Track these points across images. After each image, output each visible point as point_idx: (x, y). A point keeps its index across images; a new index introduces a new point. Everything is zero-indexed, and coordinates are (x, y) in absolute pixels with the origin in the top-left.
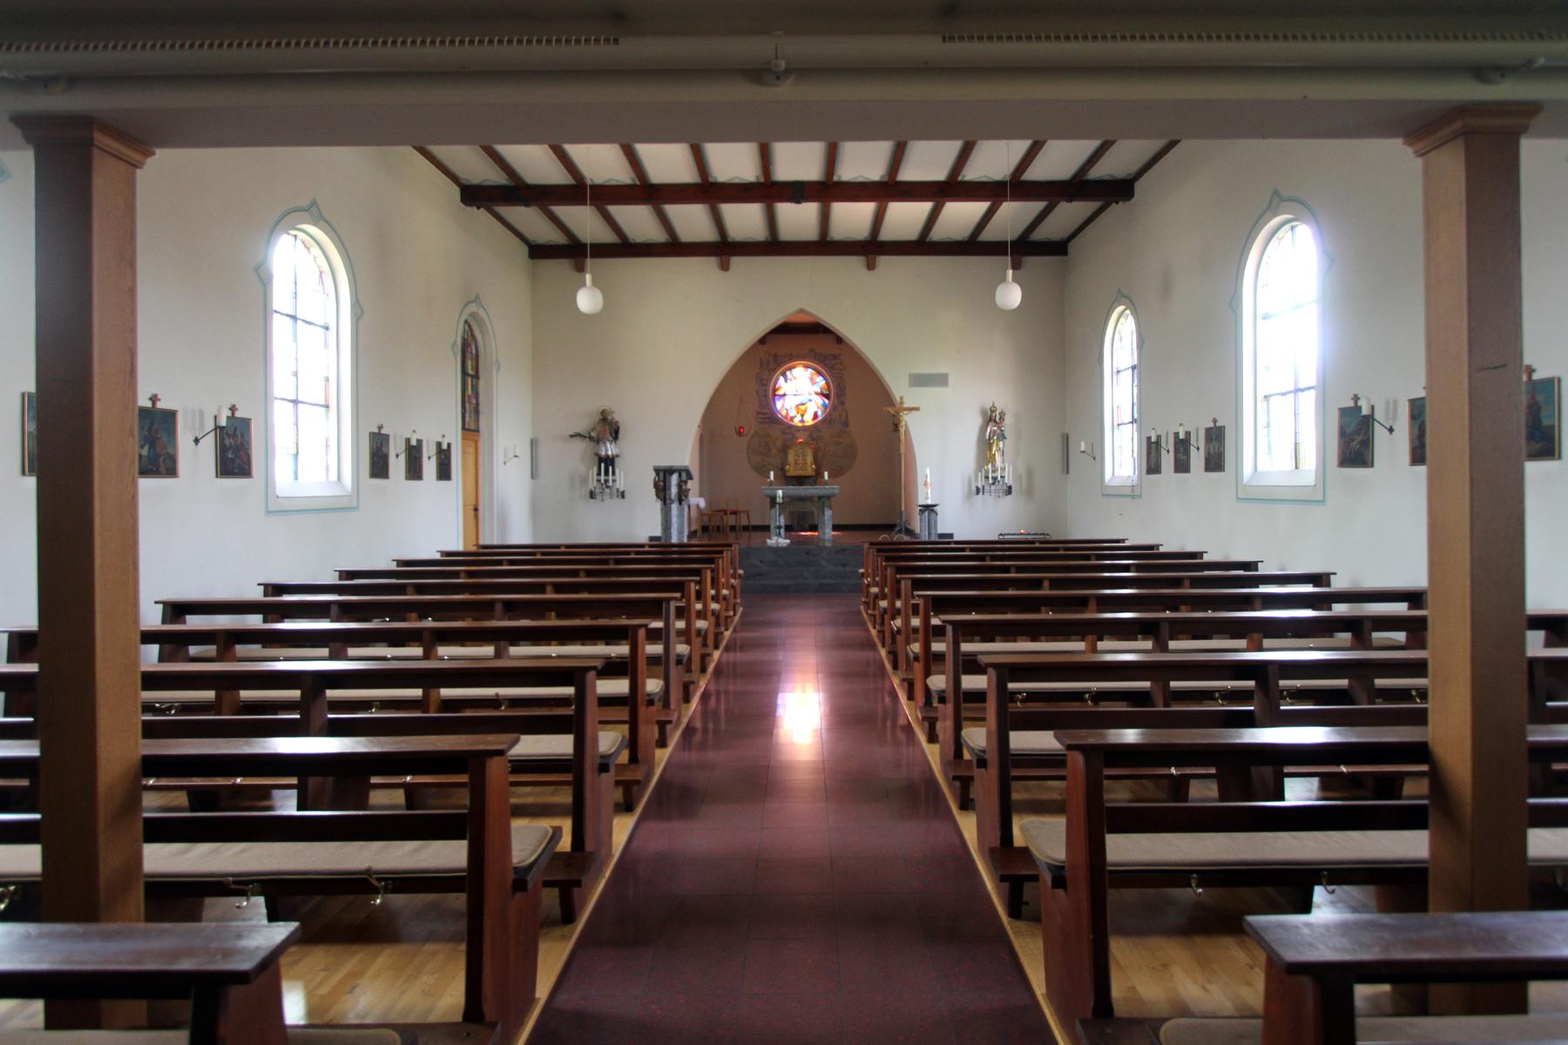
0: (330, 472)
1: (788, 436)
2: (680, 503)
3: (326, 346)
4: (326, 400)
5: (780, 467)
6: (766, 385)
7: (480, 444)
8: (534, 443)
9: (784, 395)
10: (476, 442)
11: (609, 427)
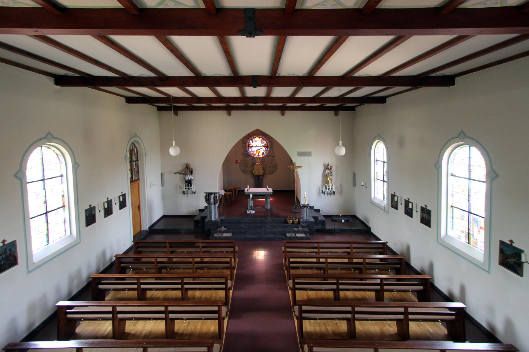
0: (66, 232)
1: (254, 161)
2: (215, 204)
3: (62, 183)
4: (63, 204)
5: (251, 171)
6: (246, 144)
7: (140, 183)
8: (162, 174)
9: (252, 147)
10: (138, 184)
11: (188, 170)
